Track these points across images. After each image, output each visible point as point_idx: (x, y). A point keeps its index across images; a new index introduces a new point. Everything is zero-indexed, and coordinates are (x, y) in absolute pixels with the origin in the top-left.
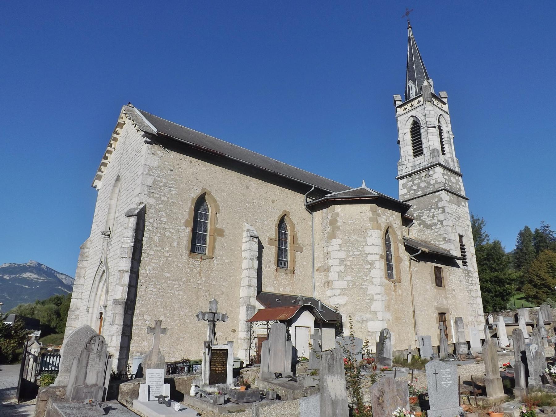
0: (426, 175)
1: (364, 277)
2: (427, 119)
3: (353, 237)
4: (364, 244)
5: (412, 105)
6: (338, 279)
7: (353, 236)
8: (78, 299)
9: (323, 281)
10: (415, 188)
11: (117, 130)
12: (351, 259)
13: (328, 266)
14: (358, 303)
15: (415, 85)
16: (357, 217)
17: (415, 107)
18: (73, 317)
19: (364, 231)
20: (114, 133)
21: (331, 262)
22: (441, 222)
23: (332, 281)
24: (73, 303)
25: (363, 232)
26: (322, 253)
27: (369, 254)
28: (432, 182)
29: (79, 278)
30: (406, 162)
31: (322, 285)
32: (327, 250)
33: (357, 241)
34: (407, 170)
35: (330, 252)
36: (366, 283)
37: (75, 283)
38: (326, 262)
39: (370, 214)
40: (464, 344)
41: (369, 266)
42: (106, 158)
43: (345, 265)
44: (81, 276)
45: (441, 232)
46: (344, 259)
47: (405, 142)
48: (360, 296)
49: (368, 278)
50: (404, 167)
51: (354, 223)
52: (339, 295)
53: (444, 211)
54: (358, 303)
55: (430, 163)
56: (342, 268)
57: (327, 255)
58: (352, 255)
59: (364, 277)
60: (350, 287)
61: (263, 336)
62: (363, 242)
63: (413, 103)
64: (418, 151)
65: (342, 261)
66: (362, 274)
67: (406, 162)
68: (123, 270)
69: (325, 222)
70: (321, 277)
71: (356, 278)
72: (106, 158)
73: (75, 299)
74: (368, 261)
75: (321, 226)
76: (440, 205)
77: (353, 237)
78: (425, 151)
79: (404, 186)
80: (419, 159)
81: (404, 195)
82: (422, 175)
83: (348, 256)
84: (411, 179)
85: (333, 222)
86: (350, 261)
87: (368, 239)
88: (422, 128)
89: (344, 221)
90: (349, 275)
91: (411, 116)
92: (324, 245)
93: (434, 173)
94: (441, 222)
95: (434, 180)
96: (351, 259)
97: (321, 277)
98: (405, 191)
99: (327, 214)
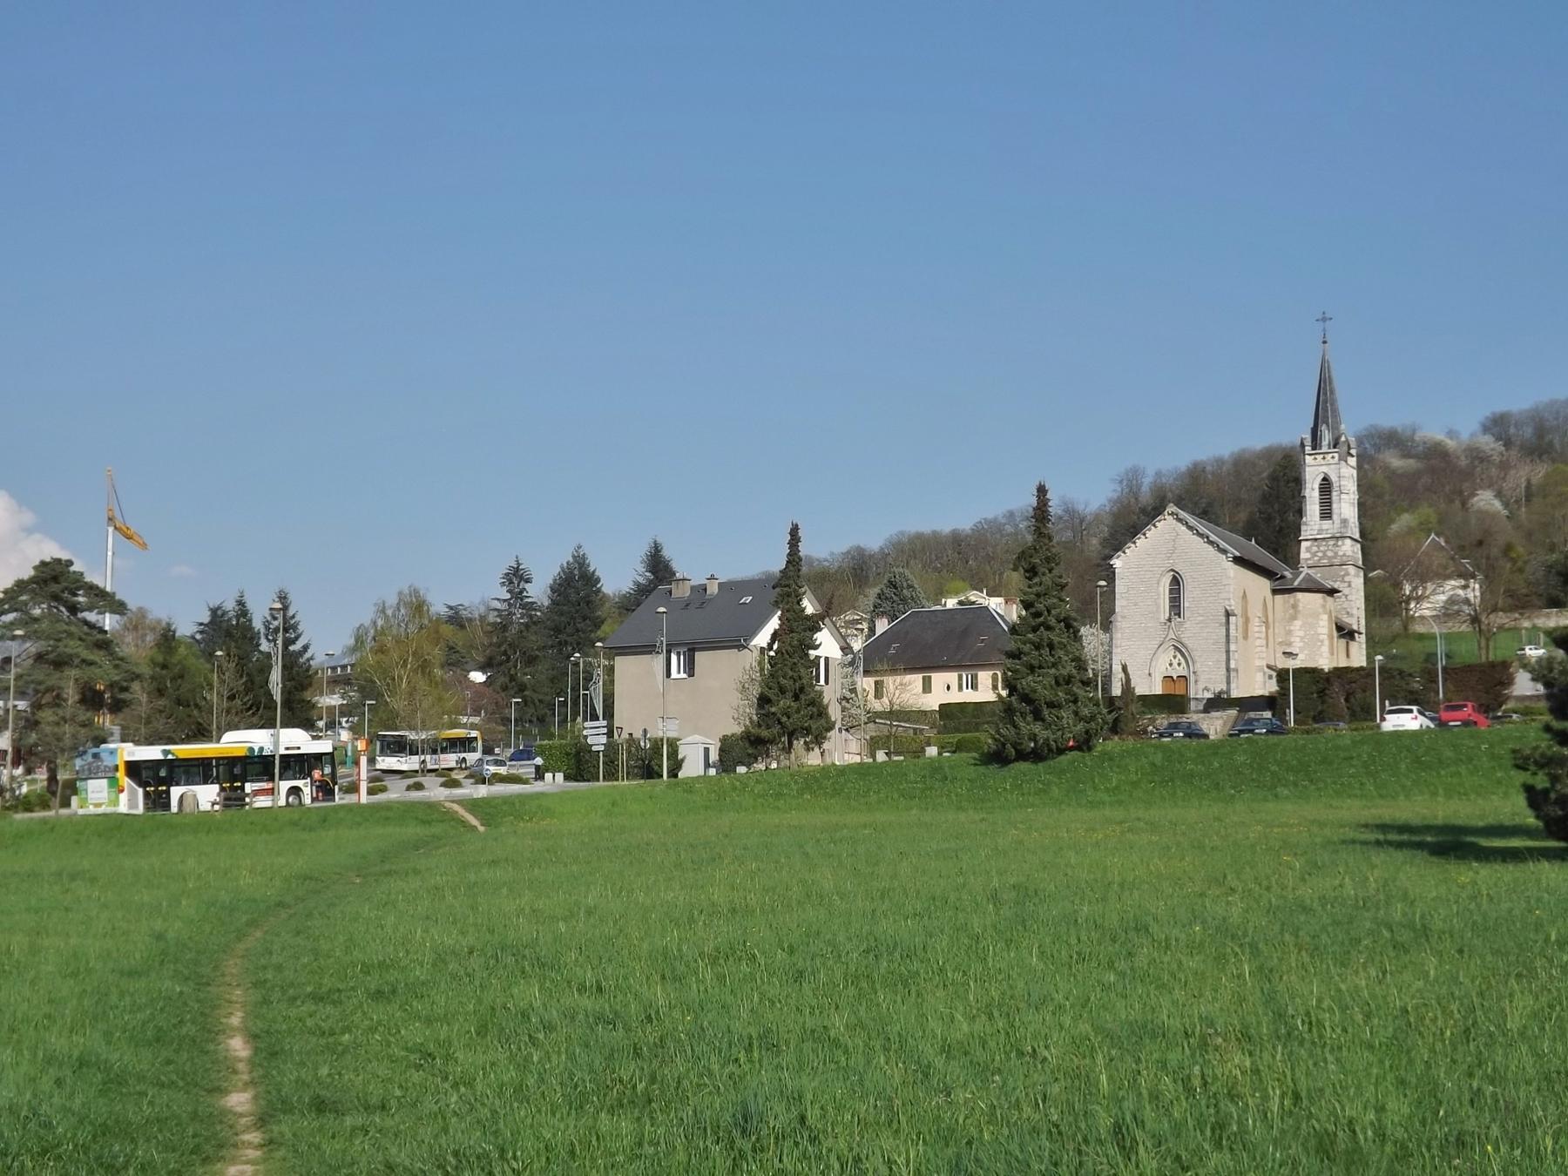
2: (1342, 483)
3: (1310, 620)
10: (1320, 554)
22: (1346, 596)
25: (1316, 616)
28: (1341, 553)
29: (1117, 647)
34: (1312, 532)
39: (1321, 601)
45: (1344, 606)
53: (1349, 586)
56: (1301, 644)
57: (1289, 632)
64: (1326, 514)
65: (1302, 638)
76: (1347, 579)
77: (1310, 620)
78: (1335, 517)
79: (1308, 550)
80: (1326, 524)
81: (1307, 559)
85: (1294, 607)
93: (1343, 544)
94: (1346, 596)
98: (1308, 555)
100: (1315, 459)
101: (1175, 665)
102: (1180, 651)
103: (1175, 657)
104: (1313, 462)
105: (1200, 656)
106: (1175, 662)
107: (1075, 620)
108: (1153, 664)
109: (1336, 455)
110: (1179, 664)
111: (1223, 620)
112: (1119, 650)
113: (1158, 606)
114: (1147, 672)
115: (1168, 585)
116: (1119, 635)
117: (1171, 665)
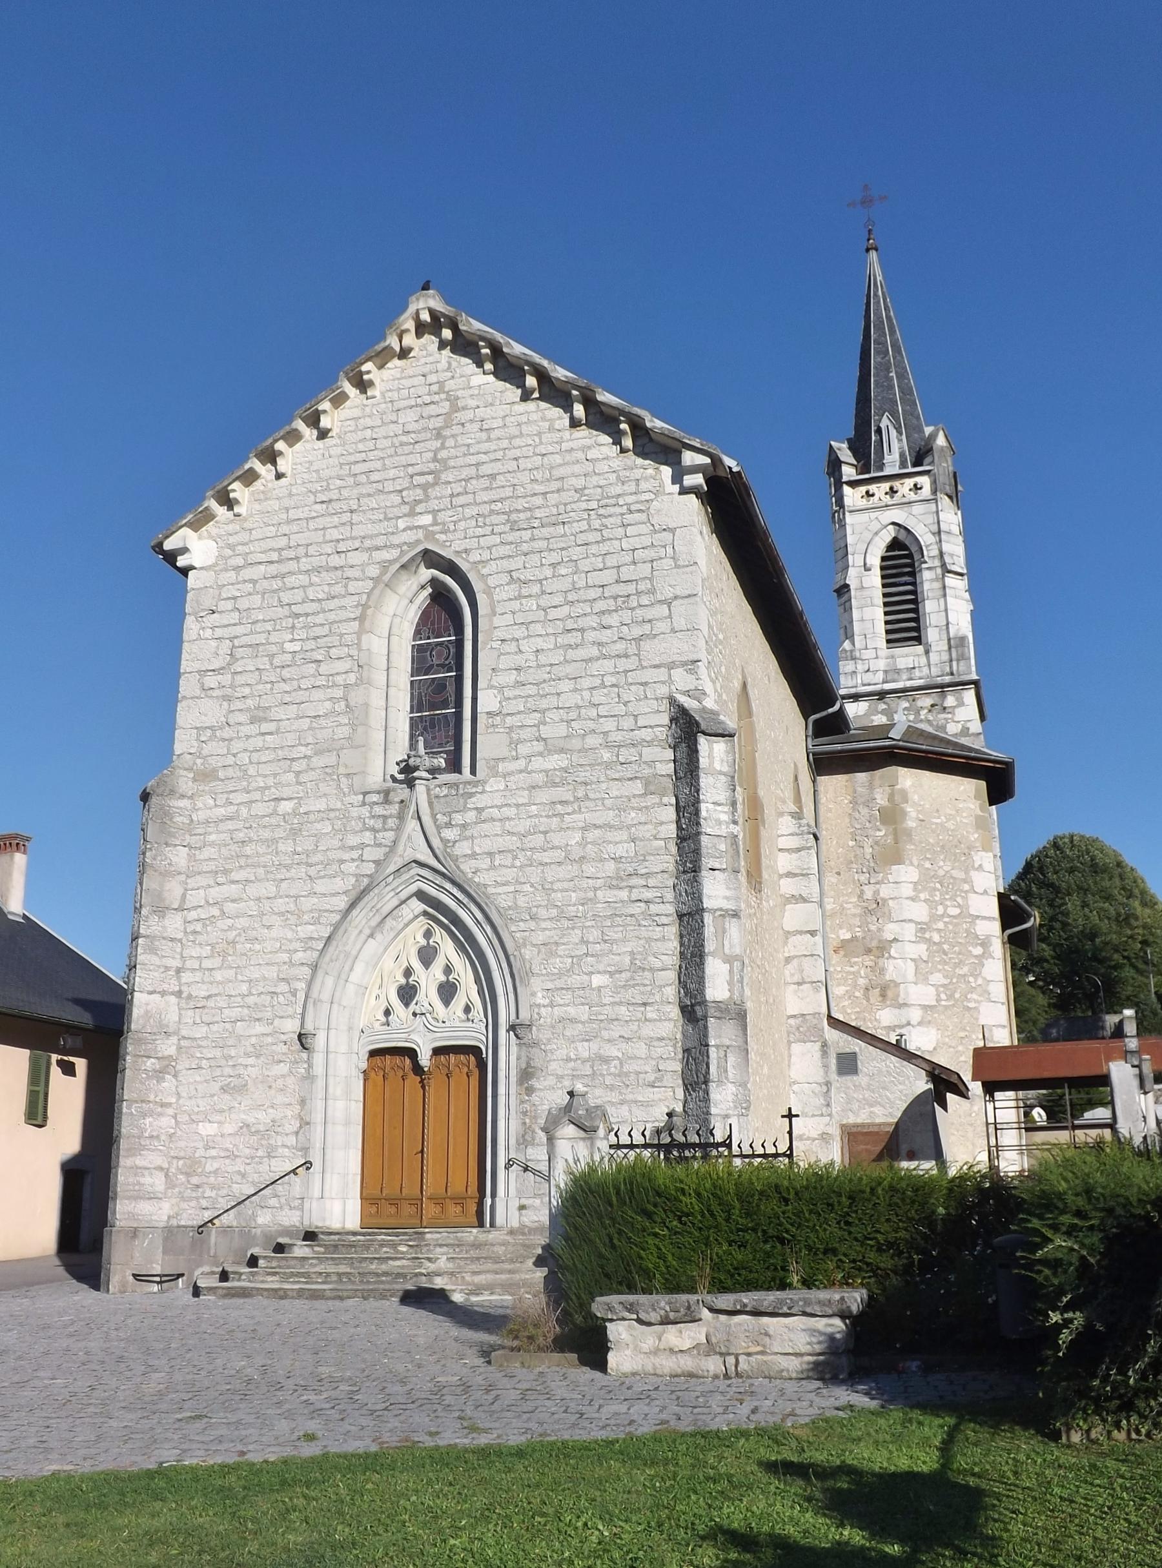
0: (932, 706)
1: (971, 979)
3: (944, 867)
4: (966, 887)
5: (893, 491)
6: (914, 980)
7: (941, 863)
8: (163, 993)
9: (862, 982)
11: (364, 368)
12: (940, 925)
13: (880, 941)
14: (960, 1048)
15: (900, 433)
16: (949, 811)
17: (904, 500)
18: (150, 1063)
19: (966, 851)
20: (346, 374)
21: (890, 930)
23: (897, 985)
24: (142, 1011)
26: (855, 899)
27: (978, 917)
29: (161, 911)
30: (867, 654)
31: (857, 994)
32: (877, 892)
33: (952, 877)
34: (868, 677)
35: (884, 900)
36: (974, 996)
37: (142, 931)
38: (873, 928)
40: (521, 1215)
41: (978, 951)
42: (271, 457)
43: (929, 941)
44: (167, 903)
46: (925, 924)
47: (866, 593)
48: (965, 1030)
49: (980, 981)
50: (861, 667)
51: (942, 824)
52: (920, 1024)
54: (960, 1048)
55: (947, 674)
56: (921, 950)
57: (877, 908)
58: (943, 916)
59: (971, 979)
60: (943, 1003)
61: (871, 1129)
62: (965, 881)
63: (897, 484)
65: (923, 929)
66: (965, 970)
67: (867, 654)
68: (721, 909)
69: (864, 811)
70: (852, 969)
71: (954, 980)
72: (271, 457)
73: (151, 993)
74: (977, 936)
75: (847, 820)
77: (944, 867)
78: (932, 635)
80: (908, 656)
82: (920, 703)
83: (934, 918)
84: (884, 706)
85: (891, 816)
86: (939, 931)
87: (974, 875)
88: (924, 566)
89: (921, 817)
90: (940, 971)
91: (893, 523)
92: (863, 878)
95: (960, 726)
96: (940, 925)
97: (852, 969)
99: (871, 787)
100: (869, 495)
101: (428, 993)
102: (466, 942)
103: (427, 956)
104: (863, 503)
105: (549, 948)
106: (428, 980)
107: (558, 1186)
108: (326, 985)
109: (924, 481)
110: (447, 991)
111: (663, 761)
112: (173, 924)
113: (357, 716)
114: (292, 1026)
115: (407, 627)
116: (179, 857)
117: (407, 993)
